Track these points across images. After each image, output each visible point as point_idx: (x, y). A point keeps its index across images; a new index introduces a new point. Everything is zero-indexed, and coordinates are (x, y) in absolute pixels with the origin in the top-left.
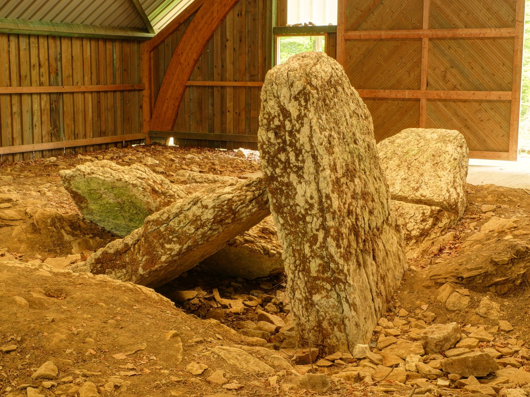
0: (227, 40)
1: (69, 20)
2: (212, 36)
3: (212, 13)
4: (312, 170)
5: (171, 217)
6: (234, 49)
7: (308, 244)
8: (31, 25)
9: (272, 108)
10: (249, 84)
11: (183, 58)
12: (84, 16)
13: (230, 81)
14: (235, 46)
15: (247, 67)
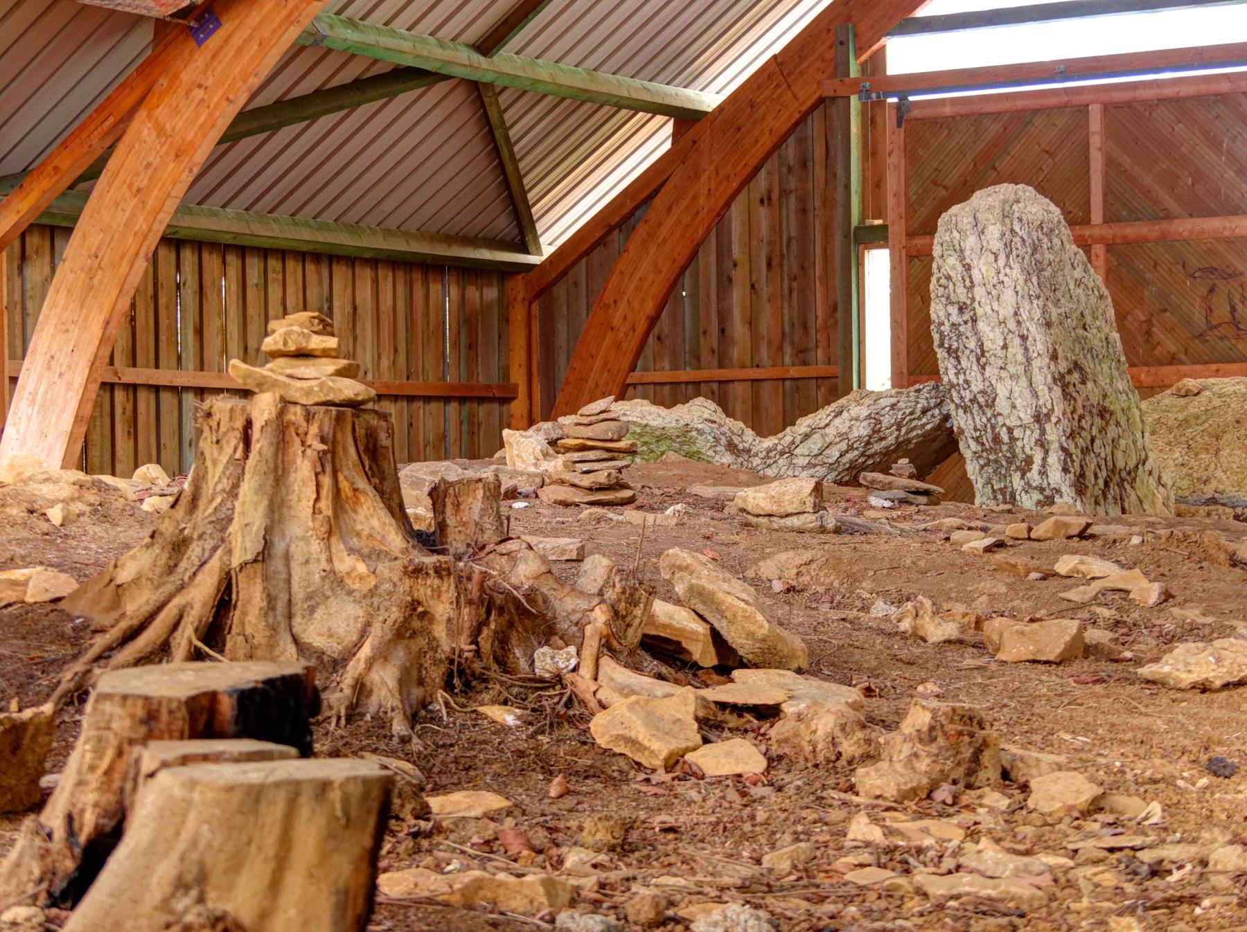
0: (735, 265)
1: (351, 217)
2: (693, 256)
3: (695, 198)
4: (1020, 358)
5: (798, 441)
6: (753, 287)
7: (1019, 473)
8: (275, 227)
9: (953, 268)
10: (794, 372)
11: (619, 314)
12: (388, 206)
13: (743, 367)
14: (754, 278)
15: (787, 329)
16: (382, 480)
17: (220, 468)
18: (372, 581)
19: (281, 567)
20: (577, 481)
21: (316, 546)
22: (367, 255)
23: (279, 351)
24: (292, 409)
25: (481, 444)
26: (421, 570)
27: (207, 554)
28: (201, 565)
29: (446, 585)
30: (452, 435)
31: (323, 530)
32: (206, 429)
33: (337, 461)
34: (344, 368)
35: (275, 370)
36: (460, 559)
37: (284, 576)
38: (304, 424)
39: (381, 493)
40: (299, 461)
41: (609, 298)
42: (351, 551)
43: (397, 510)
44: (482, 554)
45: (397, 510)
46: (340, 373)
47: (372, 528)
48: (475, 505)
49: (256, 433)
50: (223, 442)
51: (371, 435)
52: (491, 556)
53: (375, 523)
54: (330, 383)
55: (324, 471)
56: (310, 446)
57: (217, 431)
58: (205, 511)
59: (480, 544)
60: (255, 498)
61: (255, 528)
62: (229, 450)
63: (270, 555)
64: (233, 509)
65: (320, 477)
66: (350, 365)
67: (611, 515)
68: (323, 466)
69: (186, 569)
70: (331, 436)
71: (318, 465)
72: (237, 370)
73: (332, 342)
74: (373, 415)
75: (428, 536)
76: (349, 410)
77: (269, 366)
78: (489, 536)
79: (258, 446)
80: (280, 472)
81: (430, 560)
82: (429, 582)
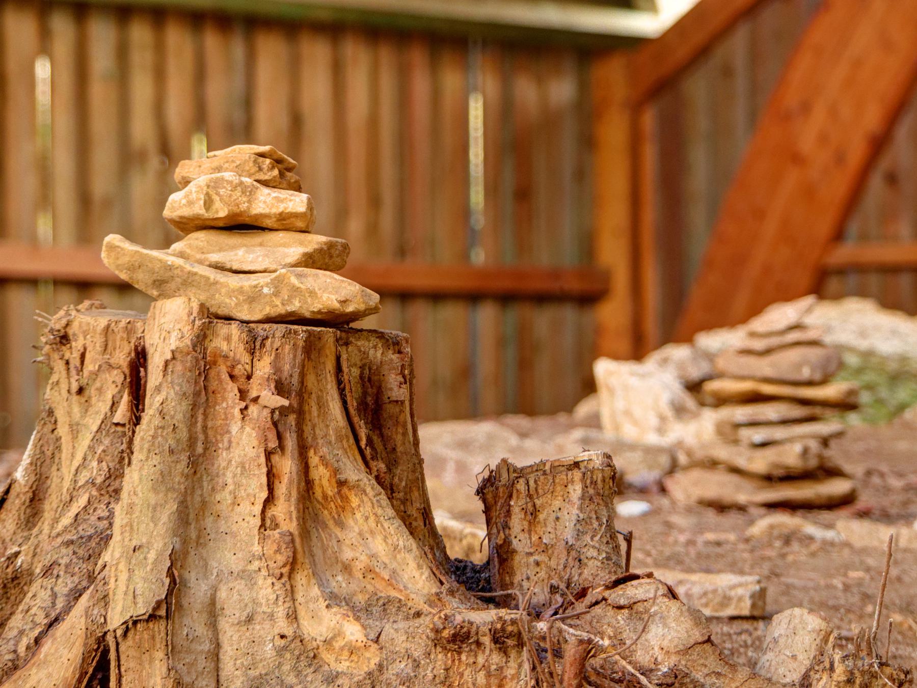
16: (392, 465)
17: (85, 440)
18: (373, 658)
19: (201, 629)
20: (741, 462)
21: (266, 591)
22: (323, 15)
23: (197, 218)
24: (223, 329)
25: (551, 388)
26: (468, 635)
27: (60, 604)
28: (50, 625)
29: (513, 664)
30: (485, 365)
31: (281, 559)
32: (59, 366)
33: (307, 429)
34: (320, 251)
35: (193, 253)
36: (538, 616)
37: (207, 646)
38: (246, 358)
39: (390, 490)
40: (235, 428)
41: (791, 98)
42: (333, 599)
43: (417, 519)
44: (580, 607)
45: (417, 519)
46: (311, 261)
47: (372, 556)
48: (565, 512)
49: (154, 376)
50: (92, 391)
51: (371, 380)
52: (598, 610)
53: (378, 546)
54: (294, 280)
55: (281, 447)
56: (256, 400)
57: (80, 370)
58: (57, 520)
59: (577, 589)
60: (153, 499)
61: (152, 556)
62: (102, 407)
63: (180, 606)
64: (111, 517)
65: (276, 459)
66: (331, 245)
67: (810, 529)
68: (280, 437)
69: (22, 632)
70: (295, 380)
71: (272, 436)
72: (116, 252)
73: (297, 202)
74: (374, 340)
75: (474, 569)
76: (329, 334)
77: (177, 246)
78: (594, 571)
79: (159, 399)
80: (200, 449)
81: (485, 617)
82: (481, 660)
